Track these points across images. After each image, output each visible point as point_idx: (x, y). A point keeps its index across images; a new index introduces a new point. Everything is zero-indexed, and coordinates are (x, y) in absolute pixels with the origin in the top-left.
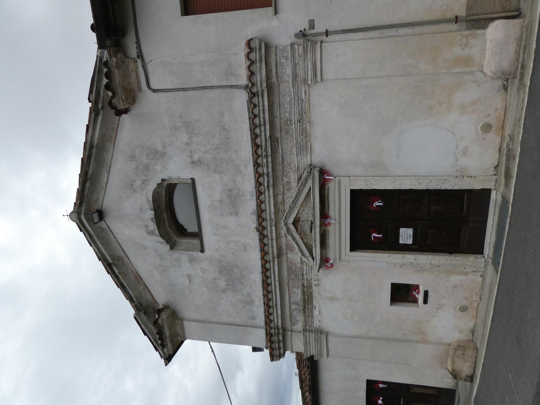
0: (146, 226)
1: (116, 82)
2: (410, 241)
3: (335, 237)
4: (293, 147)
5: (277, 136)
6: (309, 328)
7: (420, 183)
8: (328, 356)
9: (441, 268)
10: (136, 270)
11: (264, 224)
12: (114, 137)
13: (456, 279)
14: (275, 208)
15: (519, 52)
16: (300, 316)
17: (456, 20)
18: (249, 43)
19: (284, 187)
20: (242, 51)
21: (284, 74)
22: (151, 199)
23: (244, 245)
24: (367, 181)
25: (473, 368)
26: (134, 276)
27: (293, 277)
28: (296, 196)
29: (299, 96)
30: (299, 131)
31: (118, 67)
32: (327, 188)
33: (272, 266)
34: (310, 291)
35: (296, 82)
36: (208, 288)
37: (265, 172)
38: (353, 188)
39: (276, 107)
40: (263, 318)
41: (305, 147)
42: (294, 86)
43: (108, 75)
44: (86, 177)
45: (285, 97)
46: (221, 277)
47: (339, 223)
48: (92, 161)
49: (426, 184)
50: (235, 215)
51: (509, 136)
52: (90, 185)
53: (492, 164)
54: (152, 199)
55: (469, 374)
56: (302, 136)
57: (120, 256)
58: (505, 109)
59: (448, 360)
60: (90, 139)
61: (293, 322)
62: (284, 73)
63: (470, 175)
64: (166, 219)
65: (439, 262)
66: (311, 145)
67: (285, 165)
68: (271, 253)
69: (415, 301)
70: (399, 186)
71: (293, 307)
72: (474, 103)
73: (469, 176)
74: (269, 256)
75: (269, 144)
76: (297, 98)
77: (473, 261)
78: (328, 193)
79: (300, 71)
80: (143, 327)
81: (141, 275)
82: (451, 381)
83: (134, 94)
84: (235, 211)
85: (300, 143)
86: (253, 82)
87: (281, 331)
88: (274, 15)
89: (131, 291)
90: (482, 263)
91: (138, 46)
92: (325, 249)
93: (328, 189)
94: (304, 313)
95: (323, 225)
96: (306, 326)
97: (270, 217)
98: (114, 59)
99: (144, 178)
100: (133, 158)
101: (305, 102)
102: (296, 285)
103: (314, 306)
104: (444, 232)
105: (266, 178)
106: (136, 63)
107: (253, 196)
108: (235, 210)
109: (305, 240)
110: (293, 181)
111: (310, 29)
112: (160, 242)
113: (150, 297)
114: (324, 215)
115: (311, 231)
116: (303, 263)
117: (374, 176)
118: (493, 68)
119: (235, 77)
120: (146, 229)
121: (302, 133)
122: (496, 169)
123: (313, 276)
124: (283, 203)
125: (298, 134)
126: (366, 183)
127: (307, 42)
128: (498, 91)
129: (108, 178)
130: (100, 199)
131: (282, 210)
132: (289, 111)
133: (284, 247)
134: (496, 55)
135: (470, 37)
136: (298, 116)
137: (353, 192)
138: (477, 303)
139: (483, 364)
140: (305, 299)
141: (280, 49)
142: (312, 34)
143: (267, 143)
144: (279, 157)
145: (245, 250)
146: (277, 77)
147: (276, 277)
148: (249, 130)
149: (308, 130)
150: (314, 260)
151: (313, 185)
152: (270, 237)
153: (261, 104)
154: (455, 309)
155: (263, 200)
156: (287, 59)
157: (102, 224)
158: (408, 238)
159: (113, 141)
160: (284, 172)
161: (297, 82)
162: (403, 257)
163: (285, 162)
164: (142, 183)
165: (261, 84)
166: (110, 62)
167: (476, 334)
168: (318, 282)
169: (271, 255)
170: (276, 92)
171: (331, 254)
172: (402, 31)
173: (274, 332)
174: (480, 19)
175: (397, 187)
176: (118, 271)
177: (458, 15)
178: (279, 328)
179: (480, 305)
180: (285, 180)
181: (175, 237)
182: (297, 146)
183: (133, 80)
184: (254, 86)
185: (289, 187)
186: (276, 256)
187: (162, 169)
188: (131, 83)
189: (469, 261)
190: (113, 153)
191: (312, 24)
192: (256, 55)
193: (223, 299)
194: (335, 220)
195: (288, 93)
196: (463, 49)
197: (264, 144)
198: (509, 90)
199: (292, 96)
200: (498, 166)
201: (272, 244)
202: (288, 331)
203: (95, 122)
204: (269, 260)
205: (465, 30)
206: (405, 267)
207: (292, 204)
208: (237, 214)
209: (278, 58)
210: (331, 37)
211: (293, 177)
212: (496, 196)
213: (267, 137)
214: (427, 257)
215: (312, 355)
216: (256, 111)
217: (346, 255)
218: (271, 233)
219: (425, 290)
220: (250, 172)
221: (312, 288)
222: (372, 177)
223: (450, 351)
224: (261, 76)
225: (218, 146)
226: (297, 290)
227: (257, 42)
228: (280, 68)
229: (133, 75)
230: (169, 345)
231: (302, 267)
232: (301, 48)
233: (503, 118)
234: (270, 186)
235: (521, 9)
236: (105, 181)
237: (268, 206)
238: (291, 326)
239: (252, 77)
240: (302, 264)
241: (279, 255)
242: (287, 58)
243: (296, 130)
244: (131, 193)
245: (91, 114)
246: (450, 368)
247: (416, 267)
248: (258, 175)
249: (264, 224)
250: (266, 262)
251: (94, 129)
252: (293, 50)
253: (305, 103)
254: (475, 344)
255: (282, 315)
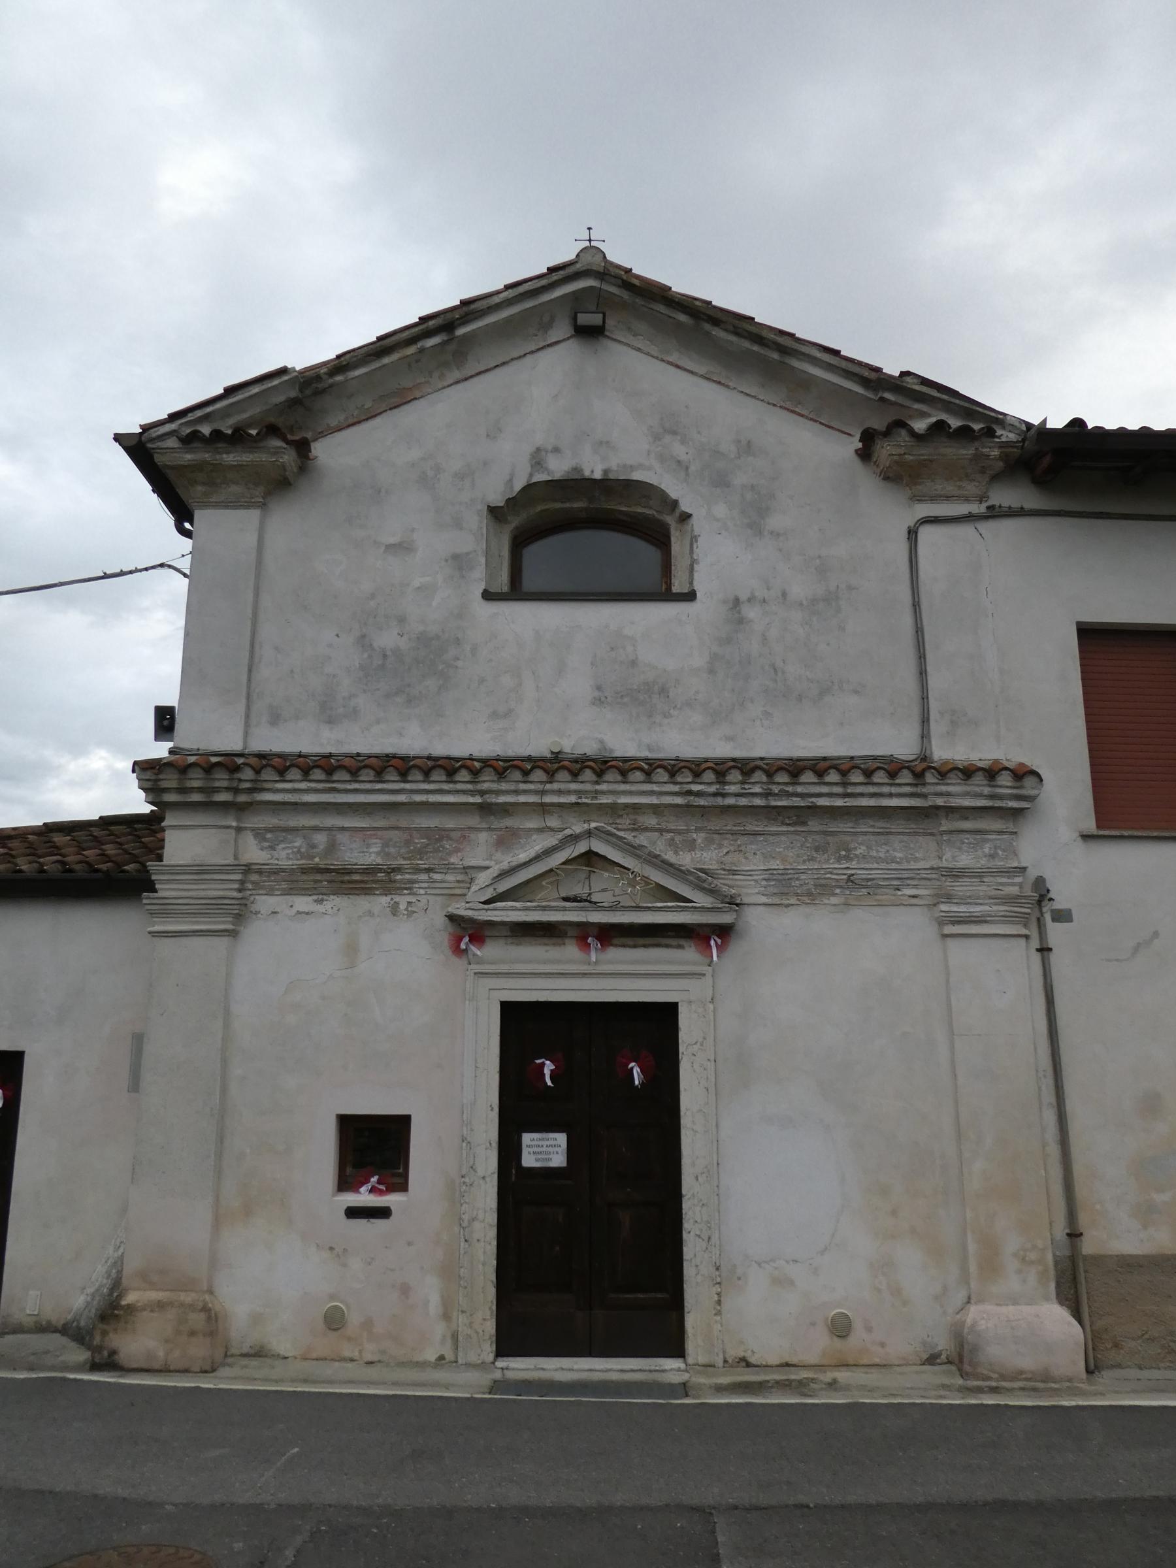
0: (556, 450)
1: (946, 447)
2: (529, 1160)
3: (545, 962)
4: (784, 860)
5: (809, 823)
6: (253, 883)
7: (699, 1178)
8: (155, 934)
9: (464, 1248)
10: (422, 397)
11: (588, 775)
12: (797, 410)
13: (430, 1291)
14: (626, 806)
15: (1020, 1380)
16: (291, 856)
17: (1074, 1235)
18: (1022, 774)
19: (680, 832)
20: (1005, 754)
21: (957, 849)
22: (637, 476)
23: (508, 714)
24: (702, 1045)
25: (144, 1365)
26: (404, 388)
27: (416, 843)
28: (671, 865)
29: (909, 882)
30: (825, 878)
31: (978, 457)
32: (682, 942)
33: (459, 786)
34: (377, 889)
35: (942, 875)
36: (373, 596)
37: (727, 787)
38: (680, 1009)
39: (880, 824)
40: (277, 748)
41: (786, 890)
42: (934, 872)
43: (964, 433)
44: (705, 318)
45: (904, 847)
46: (410, 639)
47: (586, 974)
48: (746, 344)
49: (698, 1193)
50: (594, 698)
51: (835, 1381)
52: (679, 324)
53: (752, 1351)
54: (635, 478)
55: (123, 1358)
56: (815, 885)
57: (467, 360)
58: (885, 1365)
59: (157, 1290)
60: (807, 352)
61: (269, 836)
62: (960, 849)
63: (722, 1299)
64: (567, 505)
65: (478, 1240)
66: (791, 907)
67: (738, 839)
68: (500, 788)
69: (345, 1183)
70: (688, 1126)
71: (321, 839)
72: (896, 1291)
73: (720, 1297)
74: (493, 781)
75: (797, 802)
76: (904, 876)
77: (483, 1331)
78: (667, 946)
79: (966, 886)
80: (255, 390)
81: (405, 407)
82: (28, 1312)
83: (904, 482)
84: (606, 697)
85: (798, 879)
86: (948, 775)
87: (242, 798)
88: (1080, 832)
89: (366, 374)
90: (479, 1355)
91: (1014, 511)
92: (509, 934)
93: (680, 947)
94: (304, 871)
95: (585, 934)
96: (260, 872)
97: (603, 793)
98: (996, 453)
99: (692, 468)
100: (747, 448)
101: (894, 895)
102: (392, 850)
103: (325, 897)
104: (558, 1248)
105: (713, 789)
106: (978, 501)
107: (650, 749)
108: (609, 699)
109: (546, 883)
110: (698, 856)
111: (1053, 911)
112: (511, 480)
113: (336, 423)
114: (608, 935)
115: (566, 899)
116: (466, 873)
117: (715, 1061)
118: (982, 1325)
119: (948, 733)
120: (550, 448)
121: (820, 885)
122: (738, 1362)
123: (424, 899)
124: (636, 827)
125: (819, 876)
126: (696, 1043)
127: (1030, 906)
128: (924, 1344)
129: (692, 372)
130: (632, 337)
131: (616, 823)
132: (871, 856)
133: (508, 822)
134: (1012, 1328)
135: (1040, 1268)
136: (864, 876)
137: (671, 1010)
138: (356, 1355)
139: (198, 1387)
140: (350, 872)
141: (1012, 841)
142: (1042, 916)
143: (800, 799)
144: (756, 823)
145: (494, 715)
146: (951, 832)
147: (425, 797)
148: (823, 755)
149: (829, 899)
150: (484, 903)
151: (699, 907)
152: (548, 786)
153: (894, 790)
154: (332, 1297)
155: (655, 778)
156: (990, 856)
157: (562, 329)
158: (540, 1157)
159: (788, 405)
160: (720, 834)
161: (944, 878)
162: (490, 1144)
163: (745, 838)
164: (679, 462)
165: (941, 794)
166: (991, 442)
167: (254, 1362)
168: (406, 912)
169: (494, 786)
170: (915, 827)
171: (493, 951)
172: (1050, 1117)
173: (242, 778)
174: (1076, 1287)
175: (686, 1121)
176: (428, 348)
177: (1083, 1238)
178: (255, 795)
179: (350, 1365)
180: (700, 837)
181: (515, 522)
182: (790, 872)
183: (939, 486)
184: (940, 777)
185: (680, 846)
186: (488, 800)
187: (718, 520)
188: (933, 481)
189: (484, 1320)
190: (758, 399)
191: (1063, 916)
192: (1007, 787)
193: (337, 636)
194: (596, 963)
195: (912, 855)
196: (1015, 1255)
197: (799, 789)
198: (927, 1368)
199: (906, 864)
200: (749, 1365)
201: (525, 792)
202: (238, 820)
203: (848, 375)
204: (481, 779)
205: (1054, 1255)
206: (464, 1152)
207: (650, 854)
208: (598, 702)
209: (994, 837)
210: (1036, 958)
211: (708, 857)
212: (671, 1370)
213: (813, 800)
214: (491, 1209)
215: (157, 886)
216: (879, 777)
217: (491, 991)
218: (560, 792)
219: (392, 1208)
220: (715, 749)
221: (386, 895)
222: (712, 1058)
223: (193, 1295)
224: (958, 796)
225: (780, 674)
226: (374, 852)
227: (1034, 792)
228: (971, 840)
229: (950, 488)
230: (189, 457)
231: (455, 868)
232: (1014, 890)
233: (865, 1361)
234: (688, 797)
235: (1099, 1372)
236: (680, 363)
237: (634, 788)
238: (253, 830)
239: (960, 774)
240: (463, 871)
241: (486, 809)
242: (992, 856)
243: (830, 870)
244: (651, 427)
245: (870, 369)
246: (130, 1298)
247: (463, 1179)
248: (721, 769)
249: (588, 775)
250: (475, 773)
251: (830, 367)
252: (1014, 872)
253: (892, 895)
254: (223, 1365)
255: (296, 804)
